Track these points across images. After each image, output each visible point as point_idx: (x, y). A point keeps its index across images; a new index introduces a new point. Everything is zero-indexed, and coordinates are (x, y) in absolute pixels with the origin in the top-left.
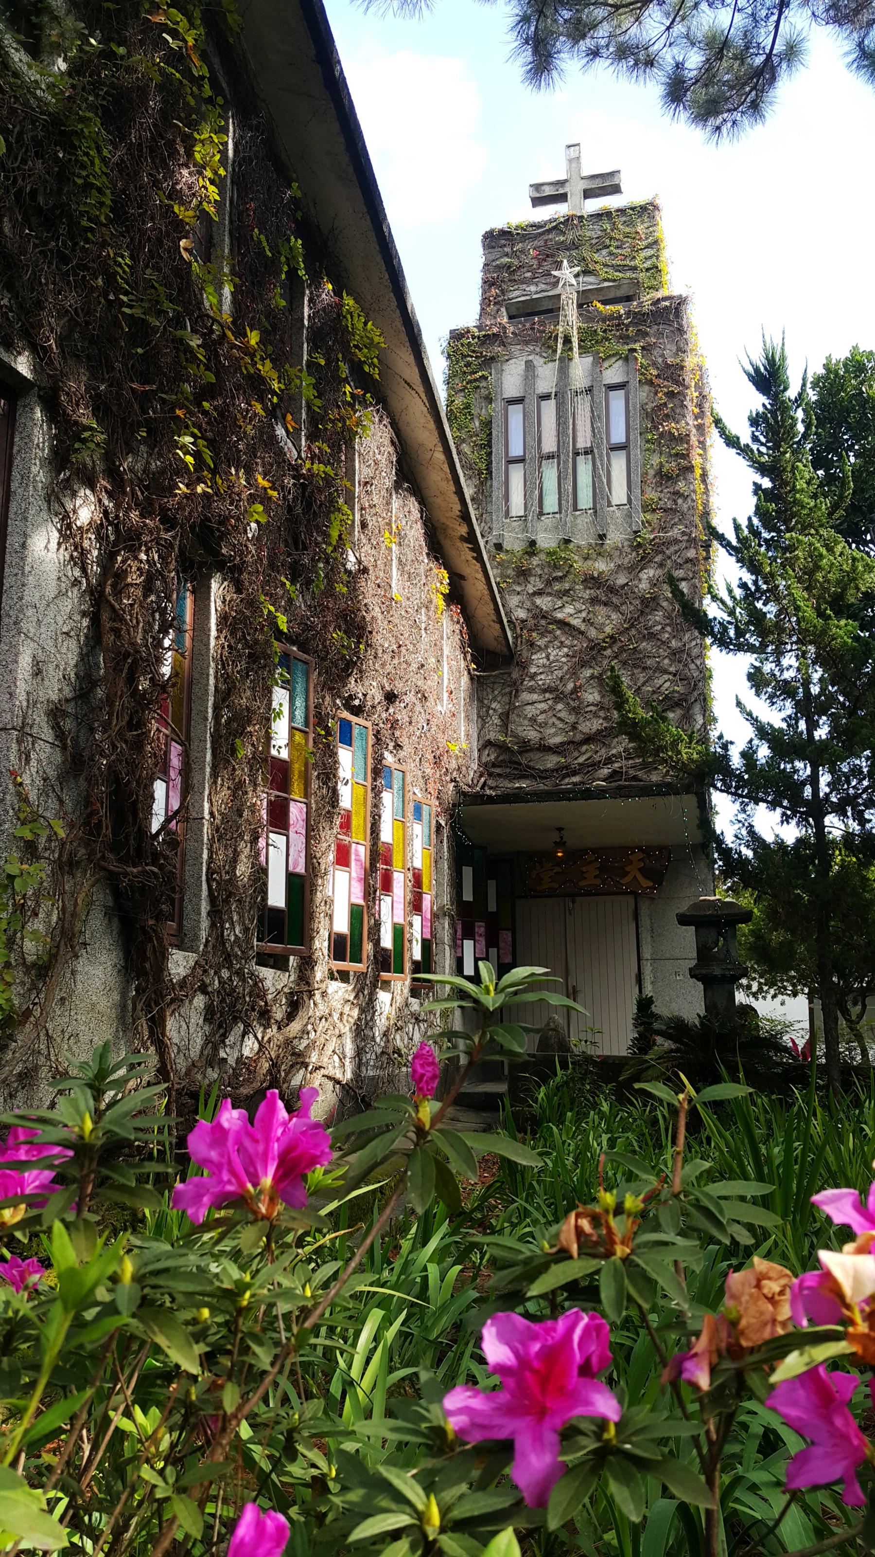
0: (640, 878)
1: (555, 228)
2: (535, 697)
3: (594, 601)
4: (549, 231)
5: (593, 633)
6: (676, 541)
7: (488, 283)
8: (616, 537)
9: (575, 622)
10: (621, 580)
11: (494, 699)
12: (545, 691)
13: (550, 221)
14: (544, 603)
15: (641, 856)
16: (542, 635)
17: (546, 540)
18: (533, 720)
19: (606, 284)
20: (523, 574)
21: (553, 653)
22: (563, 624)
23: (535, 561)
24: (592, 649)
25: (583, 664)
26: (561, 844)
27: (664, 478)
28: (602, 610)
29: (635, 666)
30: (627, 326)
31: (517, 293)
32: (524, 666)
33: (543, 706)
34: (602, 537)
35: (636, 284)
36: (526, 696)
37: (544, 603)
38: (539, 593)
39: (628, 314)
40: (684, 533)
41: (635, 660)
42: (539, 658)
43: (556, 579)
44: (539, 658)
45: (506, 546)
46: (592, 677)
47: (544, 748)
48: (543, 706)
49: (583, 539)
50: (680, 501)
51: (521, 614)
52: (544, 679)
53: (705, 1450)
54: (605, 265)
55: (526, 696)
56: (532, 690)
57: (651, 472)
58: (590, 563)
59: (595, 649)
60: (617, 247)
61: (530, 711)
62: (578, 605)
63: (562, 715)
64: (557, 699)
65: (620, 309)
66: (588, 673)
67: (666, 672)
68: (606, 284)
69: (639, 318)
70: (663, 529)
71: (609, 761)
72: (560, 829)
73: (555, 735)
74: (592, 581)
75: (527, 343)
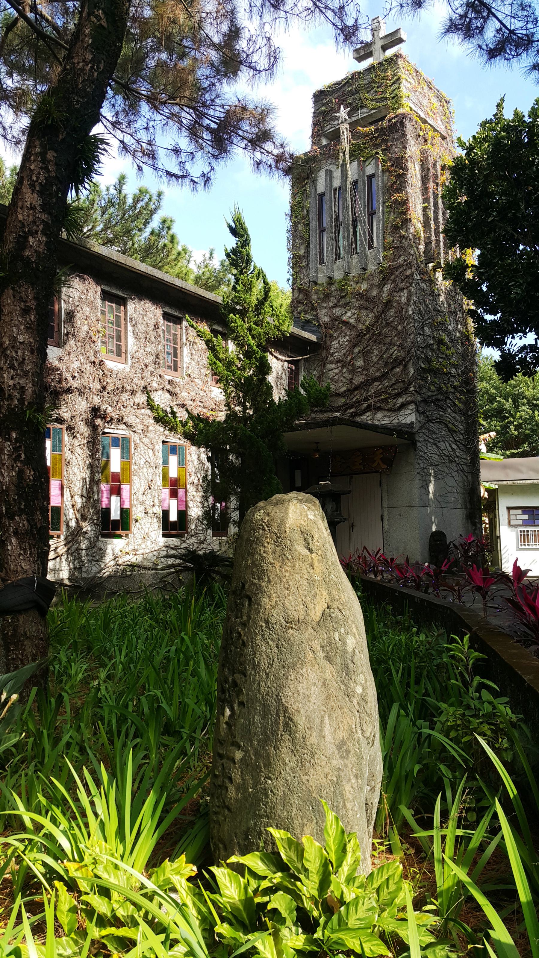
0: (381, 463)
1: (347, 82)
2: (333, 366)
3: (360, 308)
4: (344, 85)
5: (360, 326)
6: (401, 266)
7: (315, 124)
8: (372, 267)
9: (352, 321)
10: (374, 293)
11: (315, 369)
12: (337, 362)
13: (345, 79)
14: (337, 311)
15: (381, 451)
16: (336, 331)
17: (338, 275)
18: (332, 379)
19: (373, 111)
20: (327, 296)
21: (341, 339)
22: (346, 323)
23: (333, 288)
24: (359, 335)
25: (355, 345)
26: (317, 450)
27: (396, 228)
28: (364, 313)
29: (380, 343)
30: (376, 138)
31: (329, 127)
32: (328, 349)
33: (337, 371)
34: (365, 269)
35: (387, 107)
36: (329, 366)
37: (337, 311)
38: (334, 307)
39: (376, 130)
40: (405, 261)
41: (378, 339)
42: (335, 344)
43: (342, 297)
44: (335, 344)
45: (319, 281)
46: (359, 352)
47: (338, 395)
48: (337, 371)
49: (355, 272)
50: (404, 241)
51: (327, 319)
52: (337, 356)
53: (512, 790)
54: (372, 100)
55: (329, 366)
56: (332, 362)
57: (389, 225)
58: (359, 285)
59: (361, 335)
60: (378, 87)
61: (331, 374)
62: (354, 311)
63: (346, 375)
64: (343, 367)
65: (372, 128)
66: (357, 350)
67: (395, 345)
68: (373, 111)
69: (382, 131)
70: (394, 260)
71: (366, 399)
72: (317, 443)
73: (342, 386)
74: (360, 296)
75: (328, 158)
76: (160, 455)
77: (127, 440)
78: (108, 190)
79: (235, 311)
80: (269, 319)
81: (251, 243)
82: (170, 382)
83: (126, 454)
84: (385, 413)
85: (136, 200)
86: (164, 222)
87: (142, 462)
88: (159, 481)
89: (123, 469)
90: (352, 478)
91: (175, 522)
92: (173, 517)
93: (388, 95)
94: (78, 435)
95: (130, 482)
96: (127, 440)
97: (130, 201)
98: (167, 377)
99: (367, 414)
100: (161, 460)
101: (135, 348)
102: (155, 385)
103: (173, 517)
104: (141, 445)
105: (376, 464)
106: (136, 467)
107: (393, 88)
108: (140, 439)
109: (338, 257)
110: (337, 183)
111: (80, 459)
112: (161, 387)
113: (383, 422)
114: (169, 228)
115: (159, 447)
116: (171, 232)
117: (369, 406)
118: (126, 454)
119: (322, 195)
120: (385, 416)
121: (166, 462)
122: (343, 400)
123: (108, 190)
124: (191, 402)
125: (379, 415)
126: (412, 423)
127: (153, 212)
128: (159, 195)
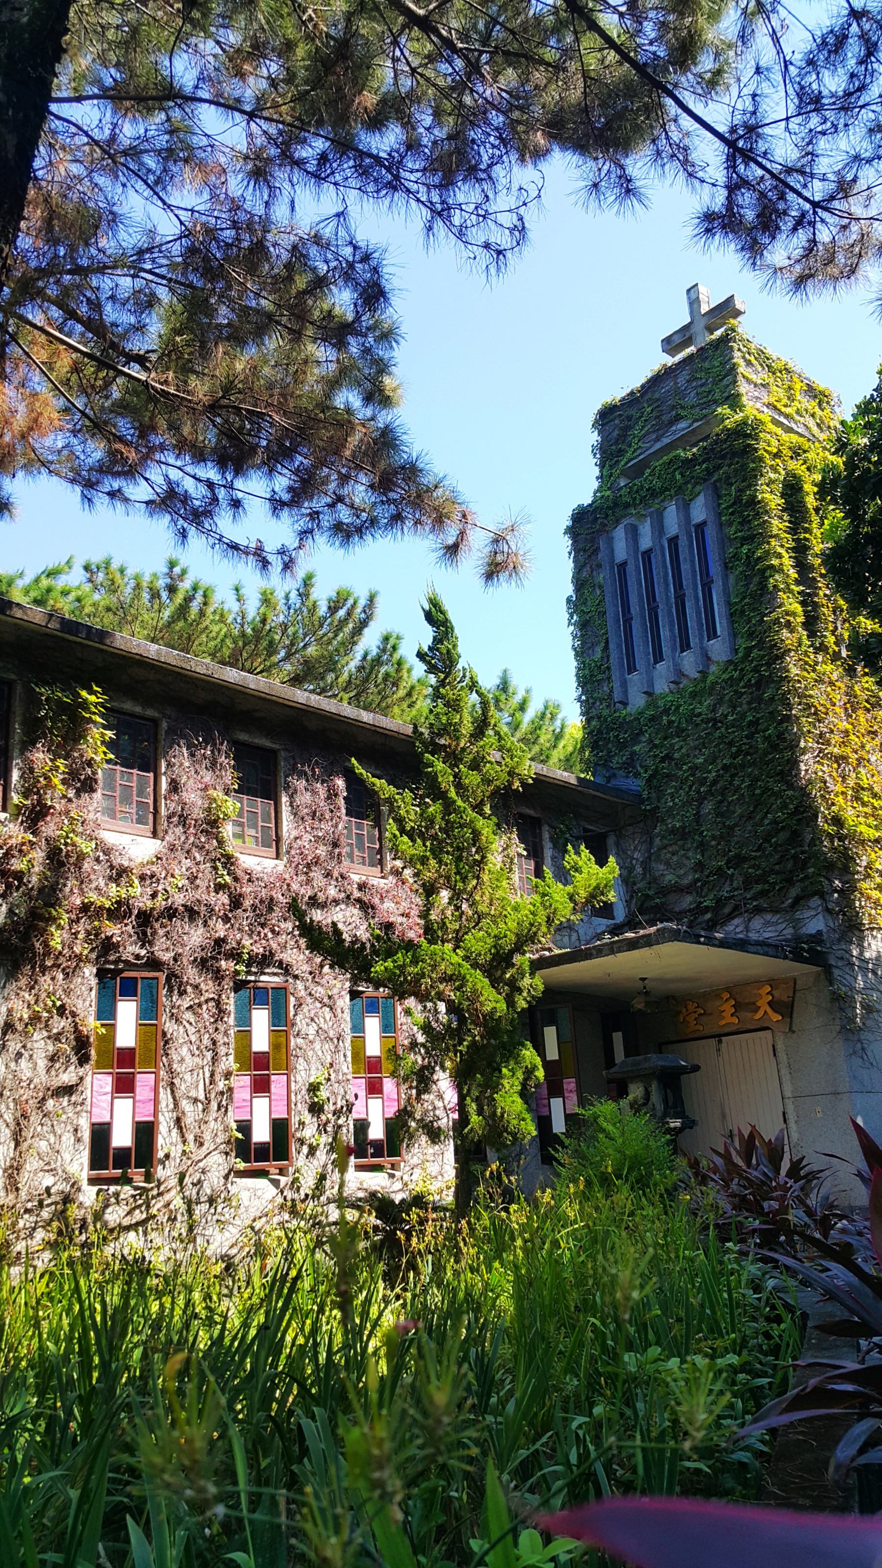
0: (769, 1010)
19: (696, 425)
68: (696, 425)
76: (347, 1016)
77: (281, 992)
78: (287, 598)
79: (436, 749)
80: (494, 756)
81: (457, 631)
82: (362, 887)
83: (280, 1019)
84: (768, 917)
85: (333, 609)
86: (386, 639)
87: (312, 1030)
88: (346, 1067)
89: (275, 1046)
90: (720, 1042)
91: (127, 1150)
92: (122, 1137)
93: (717, 396)
94: (189, 989)
95: (288, 1069)
96: (281, 992)
97: (322, 610)
98: (356, 878)
99: (736, 921)
100: (349, 1026)
101: (294, 833)
102: (332, 892)
103: (122, 1137)
104: (309, 1000)
105: (760, 1013)
106: (299, 1041)
107: (725, 382)
108: (306, 988)
109: (658, 657)
110: (646, 542)
111: (191, 1030)
112: (343, 895)
113: (767, 935)
114: (394, 648)
115: (344, 1002)
116: (396, 656)
117: (736, 908)
118: (280, 1019)
119: (624, 564)
120: (767, 924)
121: (358, 1027)
122: (689, 899)
123: (287, 598)
124: (404, 920)
125: (757, 923)
126: (820, 933)
127: (363, 624)
128: (371, 599)
